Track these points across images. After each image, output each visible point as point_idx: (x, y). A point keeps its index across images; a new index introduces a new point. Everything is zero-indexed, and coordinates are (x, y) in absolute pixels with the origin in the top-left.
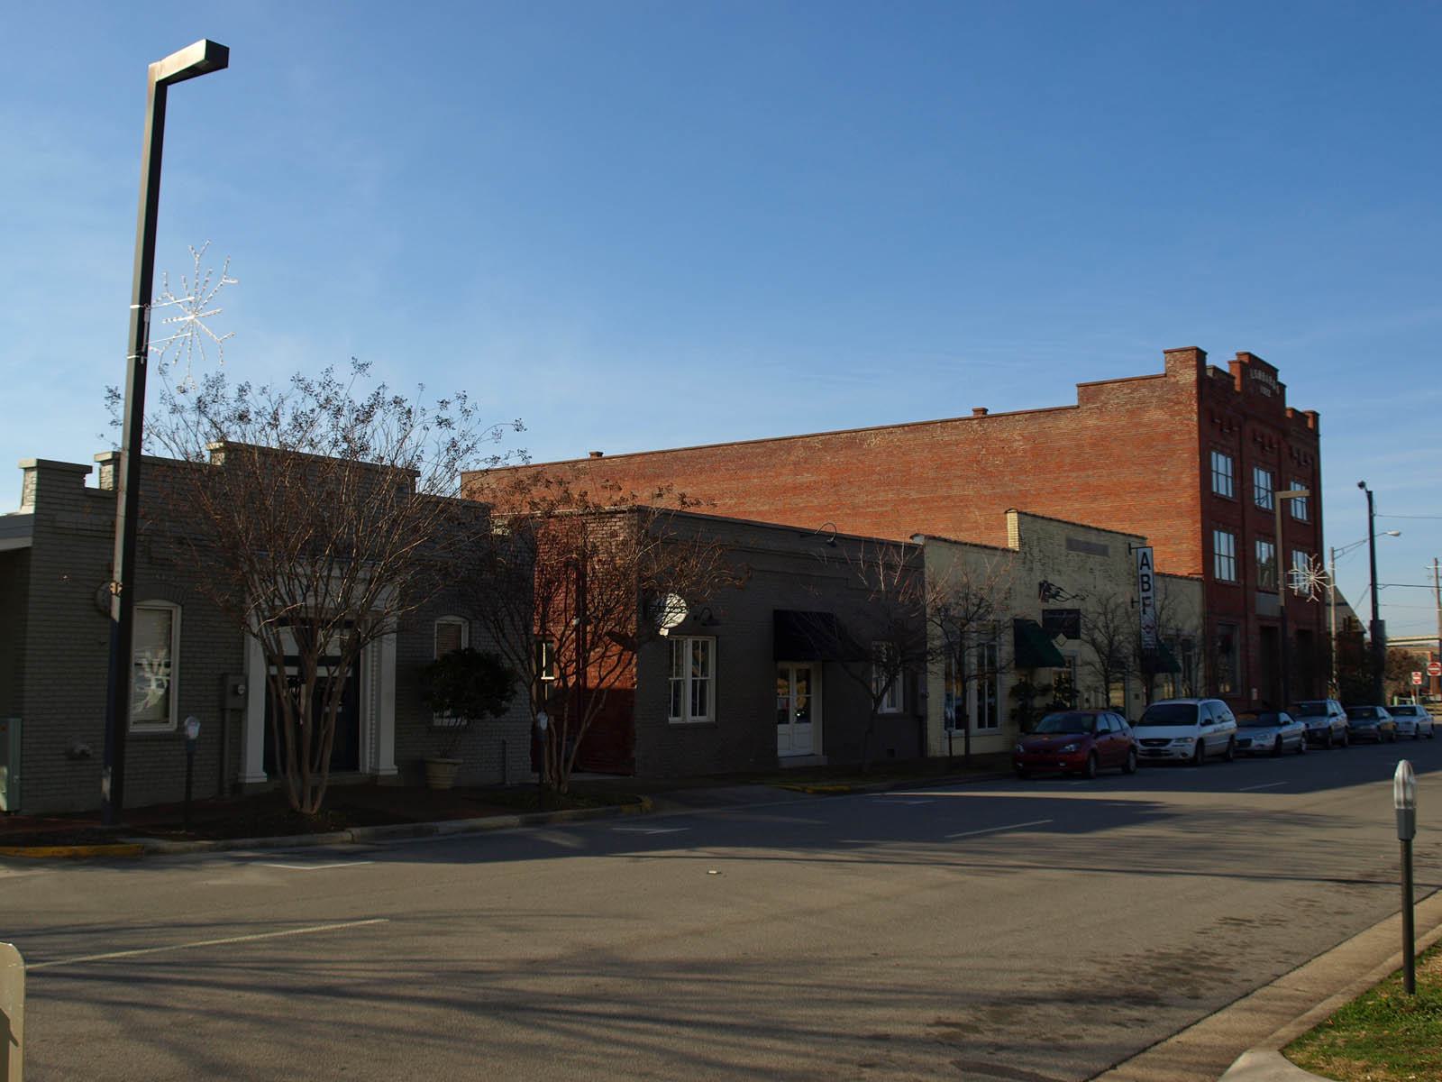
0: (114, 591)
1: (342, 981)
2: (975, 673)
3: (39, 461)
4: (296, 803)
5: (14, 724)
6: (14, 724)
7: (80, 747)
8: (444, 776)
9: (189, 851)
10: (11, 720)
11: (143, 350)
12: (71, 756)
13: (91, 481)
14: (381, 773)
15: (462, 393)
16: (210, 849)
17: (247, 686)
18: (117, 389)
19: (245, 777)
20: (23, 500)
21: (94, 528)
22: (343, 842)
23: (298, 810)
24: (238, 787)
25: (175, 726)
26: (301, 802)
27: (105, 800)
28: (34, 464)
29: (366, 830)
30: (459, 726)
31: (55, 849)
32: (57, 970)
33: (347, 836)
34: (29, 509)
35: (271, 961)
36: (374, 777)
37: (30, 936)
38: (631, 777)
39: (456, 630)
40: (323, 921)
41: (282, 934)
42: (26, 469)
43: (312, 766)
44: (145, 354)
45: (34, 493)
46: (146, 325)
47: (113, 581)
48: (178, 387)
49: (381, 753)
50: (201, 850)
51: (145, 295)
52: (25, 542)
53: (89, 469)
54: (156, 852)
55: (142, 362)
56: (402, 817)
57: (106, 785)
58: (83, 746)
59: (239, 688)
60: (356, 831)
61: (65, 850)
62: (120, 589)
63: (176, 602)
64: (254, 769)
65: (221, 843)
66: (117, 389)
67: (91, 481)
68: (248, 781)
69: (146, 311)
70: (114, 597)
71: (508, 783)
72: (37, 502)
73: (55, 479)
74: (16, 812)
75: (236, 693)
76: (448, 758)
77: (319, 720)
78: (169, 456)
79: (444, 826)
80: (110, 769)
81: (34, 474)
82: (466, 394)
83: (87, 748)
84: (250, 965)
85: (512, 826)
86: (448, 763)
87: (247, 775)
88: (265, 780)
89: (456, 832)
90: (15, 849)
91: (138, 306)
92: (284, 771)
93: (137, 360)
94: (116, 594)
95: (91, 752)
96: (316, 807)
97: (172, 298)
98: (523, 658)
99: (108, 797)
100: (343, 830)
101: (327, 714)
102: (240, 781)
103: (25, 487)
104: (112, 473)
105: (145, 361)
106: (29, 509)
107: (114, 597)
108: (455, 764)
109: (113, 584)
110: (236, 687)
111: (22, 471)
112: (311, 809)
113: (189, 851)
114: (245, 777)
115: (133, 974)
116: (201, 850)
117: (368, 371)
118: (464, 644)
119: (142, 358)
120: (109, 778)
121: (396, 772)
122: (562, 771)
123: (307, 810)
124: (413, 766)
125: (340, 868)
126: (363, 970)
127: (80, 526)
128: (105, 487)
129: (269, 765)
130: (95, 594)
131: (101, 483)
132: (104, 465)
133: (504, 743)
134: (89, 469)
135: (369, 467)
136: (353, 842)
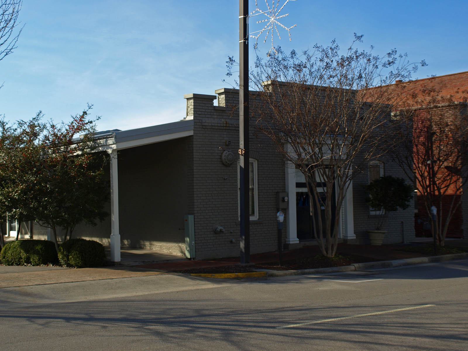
0: (240, 153)
1: (457, 333)
2: (436, 191)
3: (194, 94)
4: (325, 252)
5: (191, 218)
6: (191, 218)
7: (220, 228)
8: (378, 239)
9: (286, 275)
10: (190, 216)
11: (247, 38)
12: (216, 232)
13: (216, 103)
14: (349, 238)
15: (394, 49)
16: (295, 274)
17: (288, 197)
18: (233, 57)
19: (289, 241)
20: (187, 113)
21: (219, 125)
22: (351, 271)
23: (326, 255)
24: (287, 246)
25: (258, 217)
26: (327, 252)
27: (241, 252)
28: (192, 96)
29: (361, 265)
30: (382, 214)
31: (229, 274)
32: (306, 327)
33: (352, 267)
34: (191, 118)
35: (411, 323)
36: (345, 241)
37: (273, 312)
38: (462, 239)
39: (378, 167)
40: (403, 305)
41: (393, 311)
42: (188, 99)
43: (331, 236)
44: (248, 39)
45: (193, 110)
46: (247, 25)
47: (239, 149)
48: (267, 54)
49: (348, 228)
50: (291, 274)
51: (246, 12)
52: (191, 133)
53: (215, 97)
54: (272, 275)
55: (247, 43)
56: (368, 257)
57: (242, 245)
58: (221, 227)
59: (285, 198)
60: (356, 265)
61: (233, 275)
62: (243, 152)
63: (255, 159)
64: (293, 237)
65: (299, 271)
66: (233, 57)
67: (216, 103)
68: (291, 243)
69: (247, 19)
70: (241, 156)
71: (405, 242)
72: (194, 114)
73: (201, 102)
74: (194, 258)
75: (283, 200)
76: (379, 230)
77: (316, 212)
78: (258, 90)
79: (395, 262)
80: (244, 237)
81: (192, 101)
82: (396, 50)
83: (222, 228)
84: (398, 325)
85: (425, 263)
86: (380, 233)
87: (291, 240)
88: (298, 242)
89: (400, 266)
90: (211, 275)
91: (243, 16)
92: (319, 237)
93: (244, 43)
94: (242, 155)
95: (224, 230)
96: (334, 254)
97: (261, 11)
98: (420, 180)
99: (243, 250)
100: (350, 265)
101: (323, 211)
102: (287, 242)
103: (188, 107)
104: (224, 98)
105: (248, 43)
106: (191, 118)
107: (241, 156)
108: (384, 233)
109: (240, 150)
110: (283, 198)
111: (186, 100)
112: (332, 255)
113: (286, 275)
114: (289, 241)
115: (347, 329)
116: (291, 274)
117: (362, 39)
118: (382, 174)
119: (247, 41)
120: (244, 242)
121: (355, 238)
122: (441, 236)
123: (329, 256)
124: (363, 235)
125: (371, 282)
126: (455, 328)
127: (213, 125)
128: (221, 105)
129: (300, 235)
130: (221, 156)
131: (219, 104)
132: (220, 95)
133: (402, 222)
134: (215, 97)
135: (430, 86)
136: (355, 270)
